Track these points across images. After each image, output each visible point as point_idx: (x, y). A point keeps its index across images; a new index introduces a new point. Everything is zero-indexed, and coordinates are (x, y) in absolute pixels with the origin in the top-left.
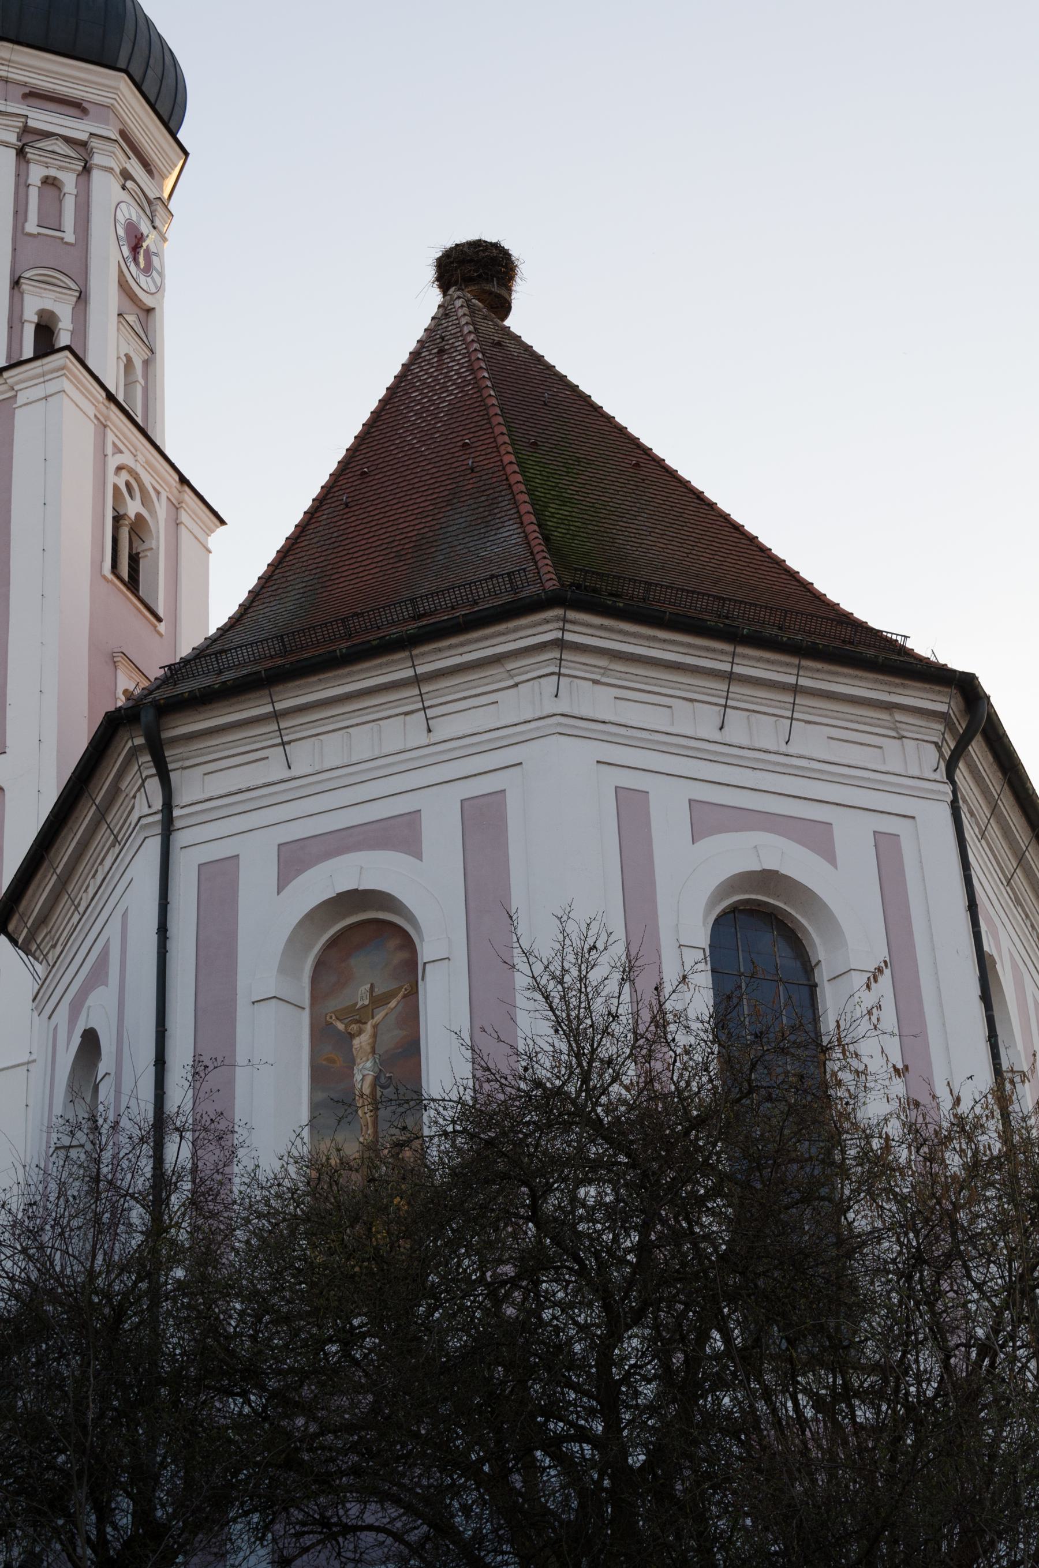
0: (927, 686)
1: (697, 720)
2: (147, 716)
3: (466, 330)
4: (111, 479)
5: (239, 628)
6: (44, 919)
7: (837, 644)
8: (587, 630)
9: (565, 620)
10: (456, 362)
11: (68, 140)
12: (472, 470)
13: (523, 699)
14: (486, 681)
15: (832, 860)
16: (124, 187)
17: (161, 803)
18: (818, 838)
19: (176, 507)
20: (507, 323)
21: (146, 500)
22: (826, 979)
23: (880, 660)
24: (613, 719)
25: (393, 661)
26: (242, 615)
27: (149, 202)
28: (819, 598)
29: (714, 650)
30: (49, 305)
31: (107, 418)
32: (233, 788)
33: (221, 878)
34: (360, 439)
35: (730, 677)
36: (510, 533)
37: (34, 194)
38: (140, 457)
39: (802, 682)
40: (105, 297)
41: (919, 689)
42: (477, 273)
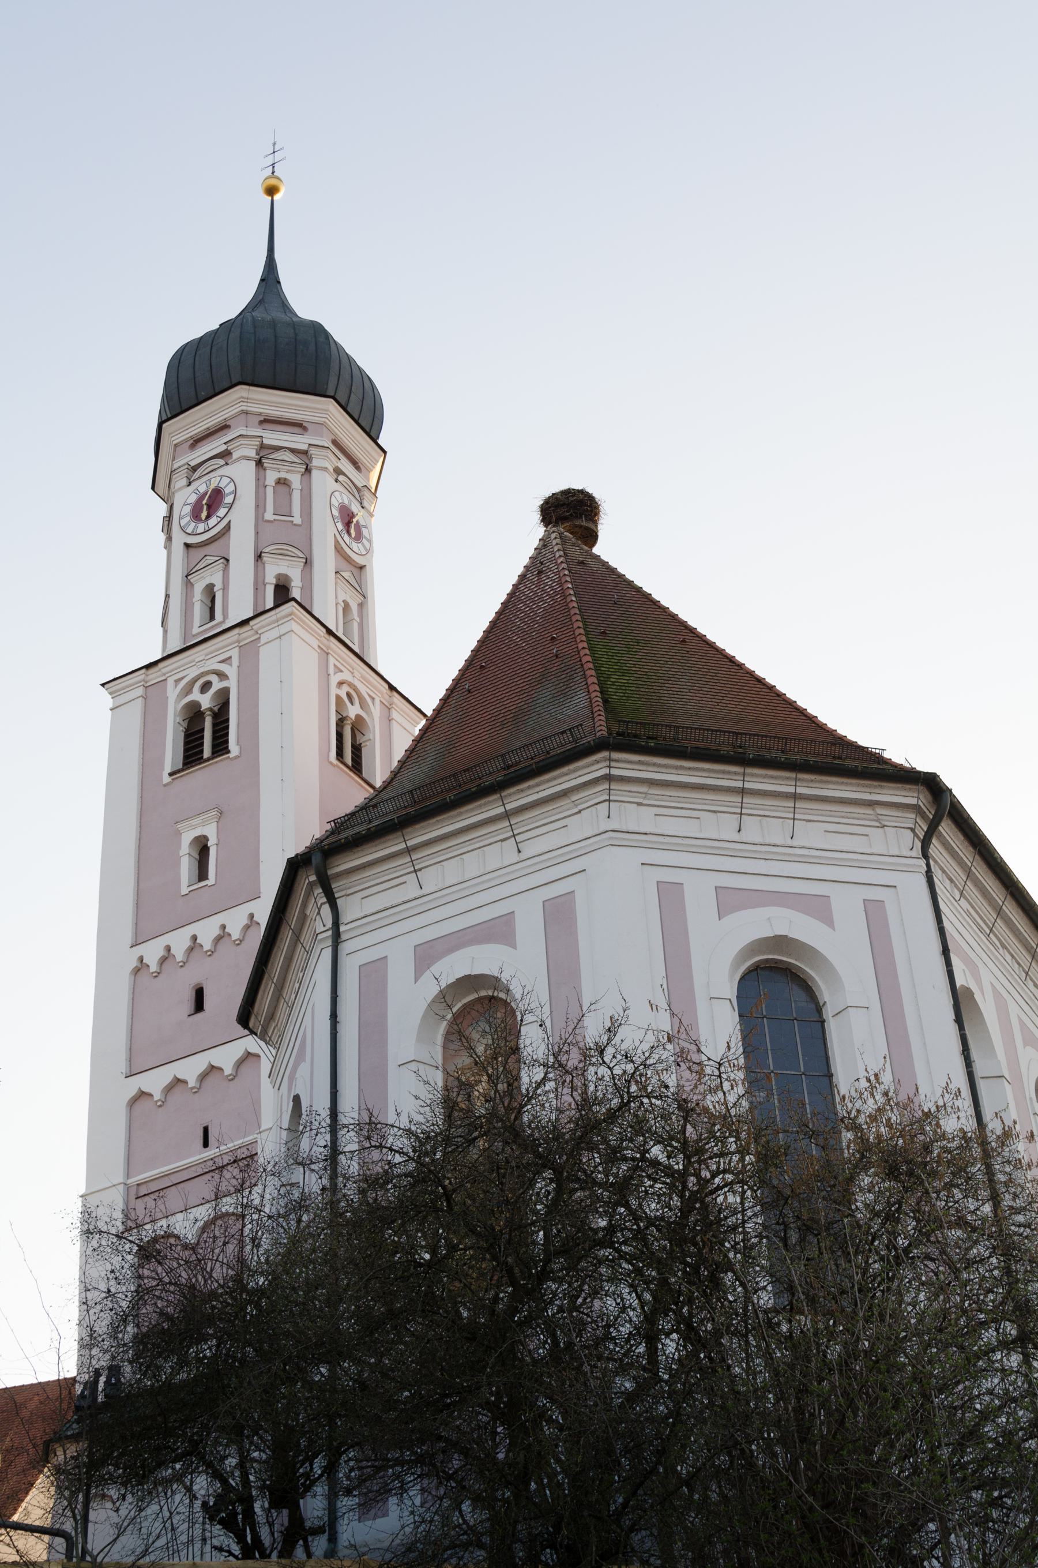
0: (900, 786)
1: (719, 825)
2: (316, 859)
3: (557, 555)
4: (334, 691)
5: (390, 788)
6: (271, 1017)
7: (829, 760)
8: (628, 765)
9: (610, 760)
10: (549, 580)
11: (293, 451)
12: (557, 656)
13: (585, 820)
14: (557, 810)
15: (830, 924)
16: (336, 481)
17: (331, 922)
18: (820, 909)
19: (388, 708)
20: (596, 550)
21: (363, 705)
22: (830, 1015)
23: (860, 769)
24: (652, 831)
25: (490, 802)
26: (392, 779)
27: (358, 490)
28: (822, 727)
29: (729, 773)
30: (283, 570)
31: (328, 647)
32: (381, 907)
33: (375, 974)
34: (482, 642)
35: (743, 792)
36: (580, 700)
37: (270, 491)
38: (356, 674)
39: (800, 790)
40: (325, 560)
41: (894, 788)
42: (571, 514)
